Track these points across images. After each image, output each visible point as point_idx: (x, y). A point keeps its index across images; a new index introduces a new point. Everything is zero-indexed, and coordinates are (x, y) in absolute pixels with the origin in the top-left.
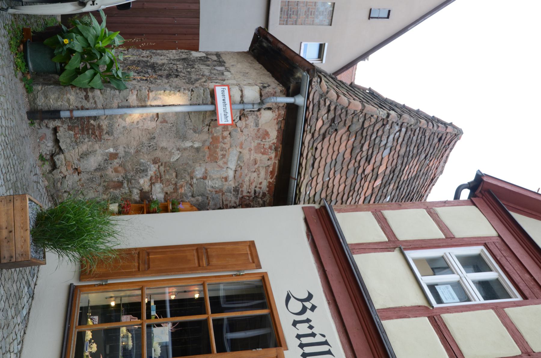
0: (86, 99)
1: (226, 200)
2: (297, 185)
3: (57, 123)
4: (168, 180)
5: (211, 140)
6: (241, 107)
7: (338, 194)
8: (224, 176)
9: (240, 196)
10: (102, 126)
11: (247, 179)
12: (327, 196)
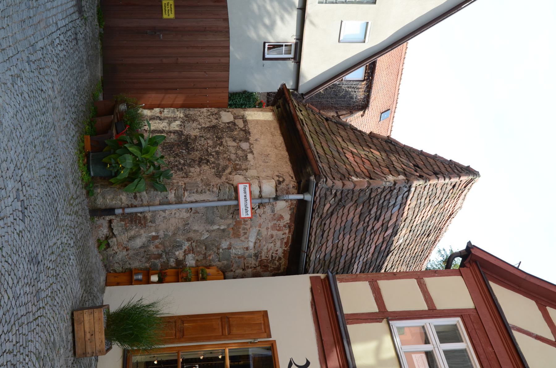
0: (135, 198)
1: (247, 263)
2: (307, 255)
3: (112, 217)
4: (198, 252)
5: (234, 223)
6: (259, 201)
7: (348, 249)
8: (246, 246)
9: (259, 259)
10: (147, 217)
11: (265, 247)
12: (337, 253)
